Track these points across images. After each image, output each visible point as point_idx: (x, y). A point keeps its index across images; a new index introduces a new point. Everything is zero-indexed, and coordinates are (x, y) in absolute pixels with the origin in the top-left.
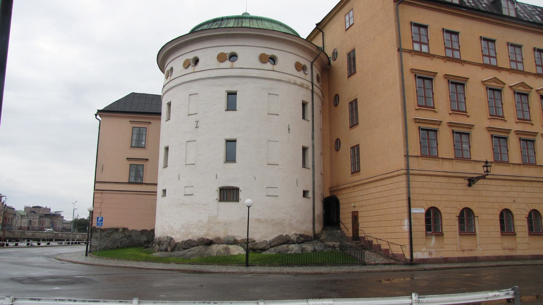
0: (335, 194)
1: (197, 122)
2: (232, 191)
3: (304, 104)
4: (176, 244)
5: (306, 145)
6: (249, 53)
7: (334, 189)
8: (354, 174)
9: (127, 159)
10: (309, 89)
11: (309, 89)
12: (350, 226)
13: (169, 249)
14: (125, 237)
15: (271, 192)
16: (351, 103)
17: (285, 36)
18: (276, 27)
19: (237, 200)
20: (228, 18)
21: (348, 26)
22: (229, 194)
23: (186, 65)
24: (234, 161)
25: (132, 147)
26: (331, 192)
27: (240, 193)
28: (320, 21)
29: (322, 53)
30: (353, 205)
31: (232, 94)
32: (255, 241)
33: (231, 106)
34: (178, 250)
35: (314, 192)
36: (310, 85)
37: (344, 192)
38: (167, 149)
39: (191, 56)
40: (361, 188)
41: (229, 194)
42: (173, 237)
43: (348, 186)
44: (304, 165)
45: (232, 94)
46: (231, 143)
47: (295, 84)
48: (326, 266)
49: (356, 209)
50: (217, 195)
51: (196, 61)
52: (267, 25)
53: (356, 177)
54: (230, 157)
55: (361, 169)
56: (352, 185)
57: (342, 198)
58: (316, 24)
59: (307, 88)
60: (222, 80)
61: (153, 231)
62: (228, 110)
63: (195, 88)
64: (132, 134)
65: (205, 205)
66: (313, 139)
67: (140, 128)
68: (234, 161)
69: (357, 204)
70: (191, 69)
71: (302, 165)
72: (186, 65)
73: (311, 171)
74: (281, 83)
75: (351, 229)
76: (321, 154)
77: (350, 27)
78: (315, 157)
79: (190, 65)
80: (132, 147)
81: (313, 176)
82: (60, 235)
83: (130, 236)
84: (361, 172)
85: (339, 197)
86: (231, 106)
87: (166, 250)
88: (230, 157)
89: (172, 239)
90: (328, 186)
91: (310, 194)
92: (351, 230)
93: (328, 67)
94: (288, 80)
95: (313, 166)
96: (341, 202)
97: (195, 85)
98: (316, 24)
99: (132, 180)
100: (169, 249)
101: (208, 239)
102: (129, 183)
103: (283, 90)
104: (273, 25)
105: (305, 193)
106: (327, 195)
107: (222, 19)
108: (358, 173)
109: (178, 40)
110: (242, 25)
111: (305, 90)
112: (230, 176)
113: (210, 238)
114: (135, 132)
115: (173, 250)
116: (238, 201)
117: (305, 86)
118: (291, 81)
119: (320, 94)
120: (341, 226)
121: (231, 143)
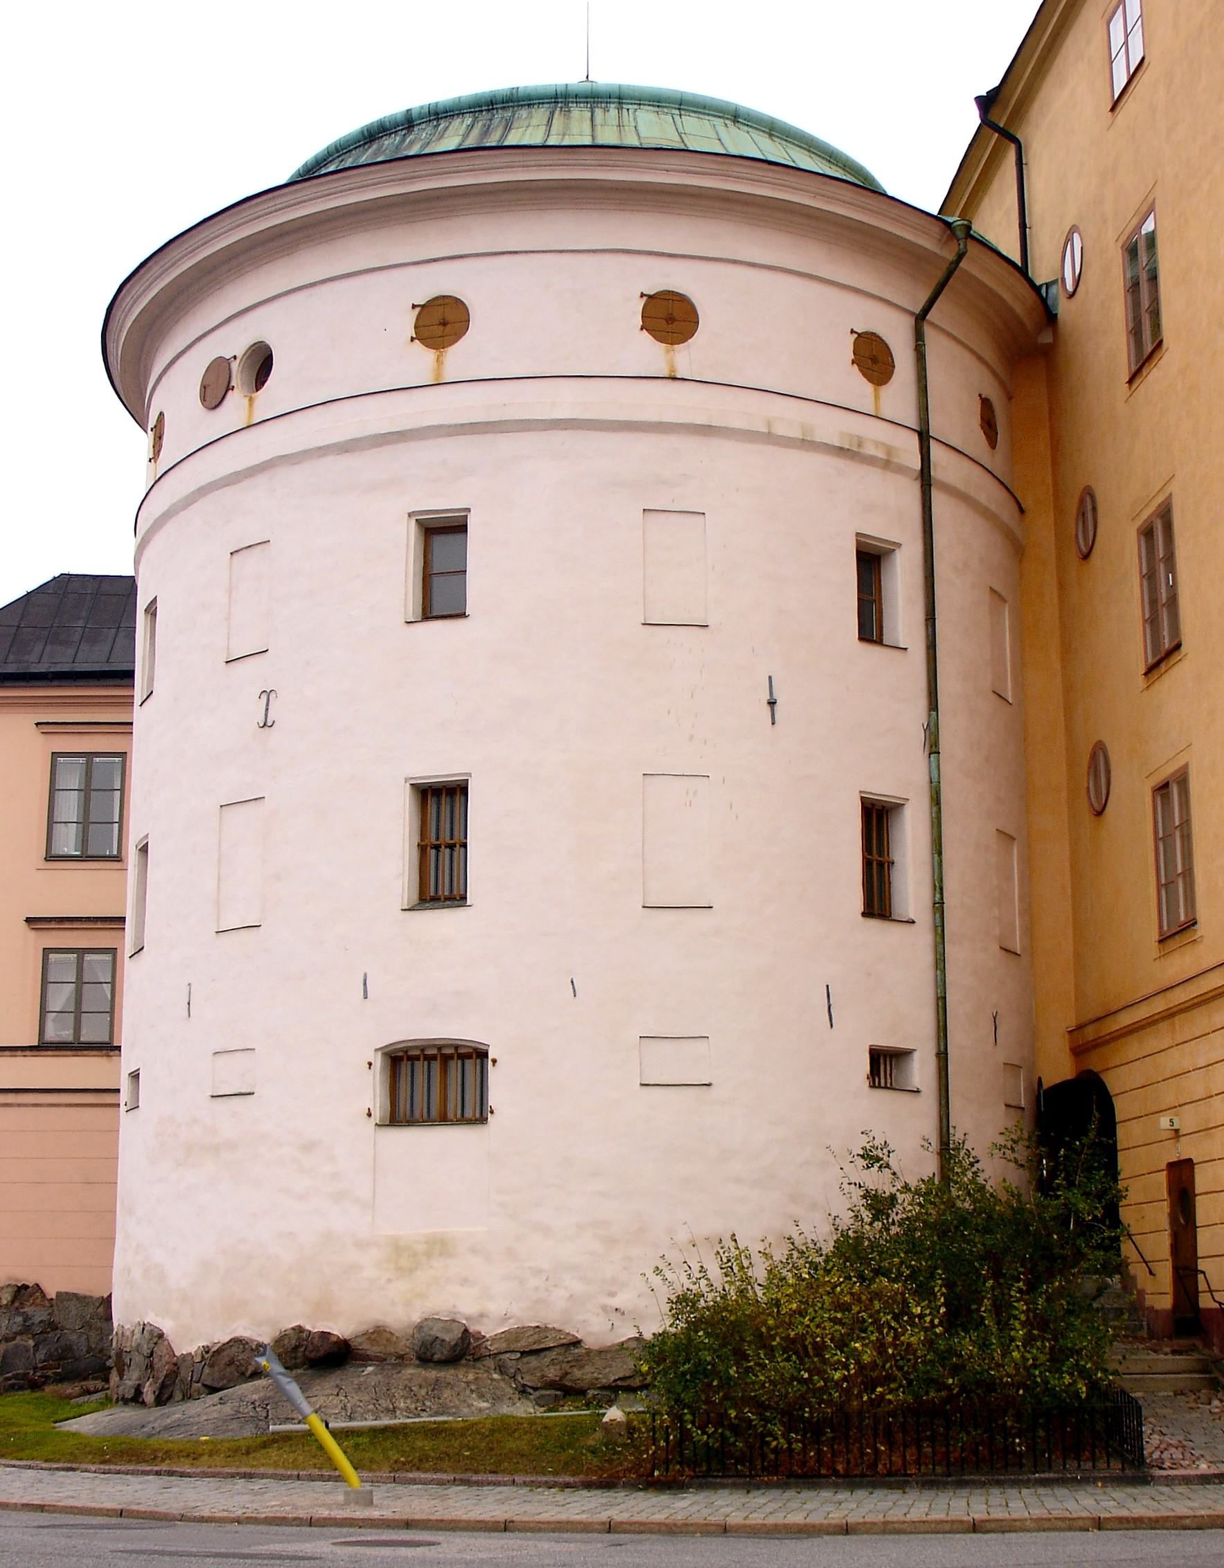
0: (1094, 1062)
1: (267, 694)
2: (455, 1066)
3: (871, 561)
4: (176, 1365)
5: (883, 789)
6: (550, 297)
7: (1090, 1033)
8: (1172, 944)
9: (28, 920)
10: (901, 470)
11: (901, 470)
12: (1159, 1245)
13: (149, 1394)
14: (26, 1329)
15: (670, 1063)
16: (1147, 533)
17: (804, 195)
18: (701, 134)
19: (476, 1114)
20: (439, 115)
21: (1120, 81)
22: (434, 1081)
23: (214, 393)
24: (457, 898)
25: (50, 857)
26: (1079, 1051)
27: (493, 1074)
28: (996, 83)
29: (973, 249)
30: (1164, 1122)
31: (442, 533)
32: (577, 1343)
33: (440, 595)
34: (187, 1397)
35: (942, 1056)
36: (911, 443)
37: (1133, 1047)
38: (144, 850)
39: (233, 343)
40: (1200, 1021)
41: (434, 1081)
42: (166, 1325)
43: (1126, 1019)
44: (878, 902)
45: (442, 533)
46: (441, 801)
47: (807, 444)
48: (902, 1486)
49: (1186, 1150)
50: (370, 1091)
51: (261, 364)
52: (652, 128)
53: (1182, 963)
54: (440, 873)
55: (1202, 913)
56: (1159, 1005)
57: (1124, 1082)
58: (980, 100)
59: (888, 465)
60: (385, 454)
61: (107, 1302)
62: (428, 614)
63: (256, 509)
64: (53, 790)
65: (309, 1147)
66: (933, 747)
67: (90, 755)
68: (457, 898)
69: (1188, 1120)
70: (235, 407)
71: (860, 907)
72: (214, 393)
73: (922, 937)
74: (716, 443)
75: (1169, 1266)
76: (1006, 837)
77: (1131, 79)
78: (958, 856)
79: (229, 388)
80: (50, 857)
81: (940, 962)
82: (792, 1334)
83: (52, 1326)
84: (1201, 929)
85: (1114, 1082)
86: (440, 595)
87: (136, 1399)
88: (440, 873)
89: (161, 1336)
90: (1058, 1023)
91: (921, 1072)
92: (1165, 1272)
93: (1046, 338)
94: (796, 434)
95: (939, 907)
96: (1122, 1108)
97: (256, 493)
98: (980, 100)
99: (58, 1031)
100: (149, 1394)
101: (325, 1335)
102: (43, 1047)
103: (728, 479)
104: (691, 123)
105: (884, 1065)
106: (1058, 1068)
107: (408, 123)
108: (1188, 937)
109: (174, 253)
110: (504, 135)
111: (873, 475)
112: (441, 980)
113: (341, 1328)
114: (72, 778)
115: (162, 1399)
116: (482, 1120)
117: (870, 450)
118: (780, 430)
119: (989, 494)
120: (1127, 1249)
121: (441, 801)
